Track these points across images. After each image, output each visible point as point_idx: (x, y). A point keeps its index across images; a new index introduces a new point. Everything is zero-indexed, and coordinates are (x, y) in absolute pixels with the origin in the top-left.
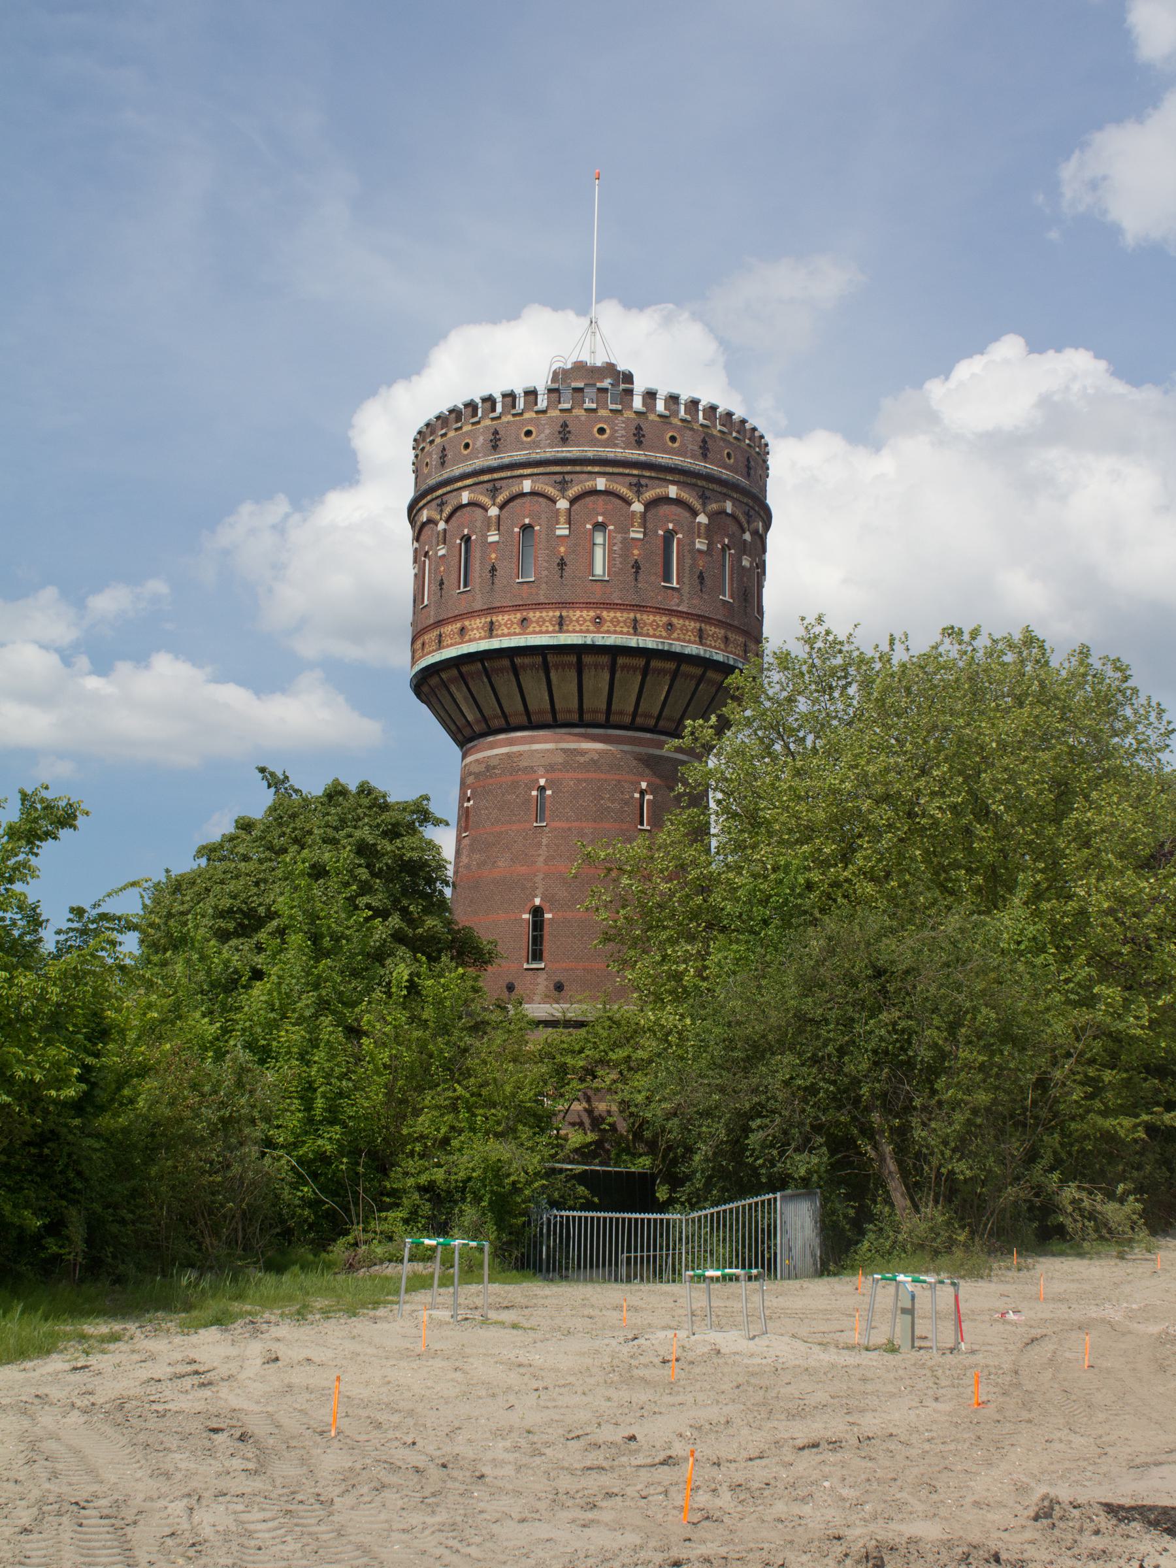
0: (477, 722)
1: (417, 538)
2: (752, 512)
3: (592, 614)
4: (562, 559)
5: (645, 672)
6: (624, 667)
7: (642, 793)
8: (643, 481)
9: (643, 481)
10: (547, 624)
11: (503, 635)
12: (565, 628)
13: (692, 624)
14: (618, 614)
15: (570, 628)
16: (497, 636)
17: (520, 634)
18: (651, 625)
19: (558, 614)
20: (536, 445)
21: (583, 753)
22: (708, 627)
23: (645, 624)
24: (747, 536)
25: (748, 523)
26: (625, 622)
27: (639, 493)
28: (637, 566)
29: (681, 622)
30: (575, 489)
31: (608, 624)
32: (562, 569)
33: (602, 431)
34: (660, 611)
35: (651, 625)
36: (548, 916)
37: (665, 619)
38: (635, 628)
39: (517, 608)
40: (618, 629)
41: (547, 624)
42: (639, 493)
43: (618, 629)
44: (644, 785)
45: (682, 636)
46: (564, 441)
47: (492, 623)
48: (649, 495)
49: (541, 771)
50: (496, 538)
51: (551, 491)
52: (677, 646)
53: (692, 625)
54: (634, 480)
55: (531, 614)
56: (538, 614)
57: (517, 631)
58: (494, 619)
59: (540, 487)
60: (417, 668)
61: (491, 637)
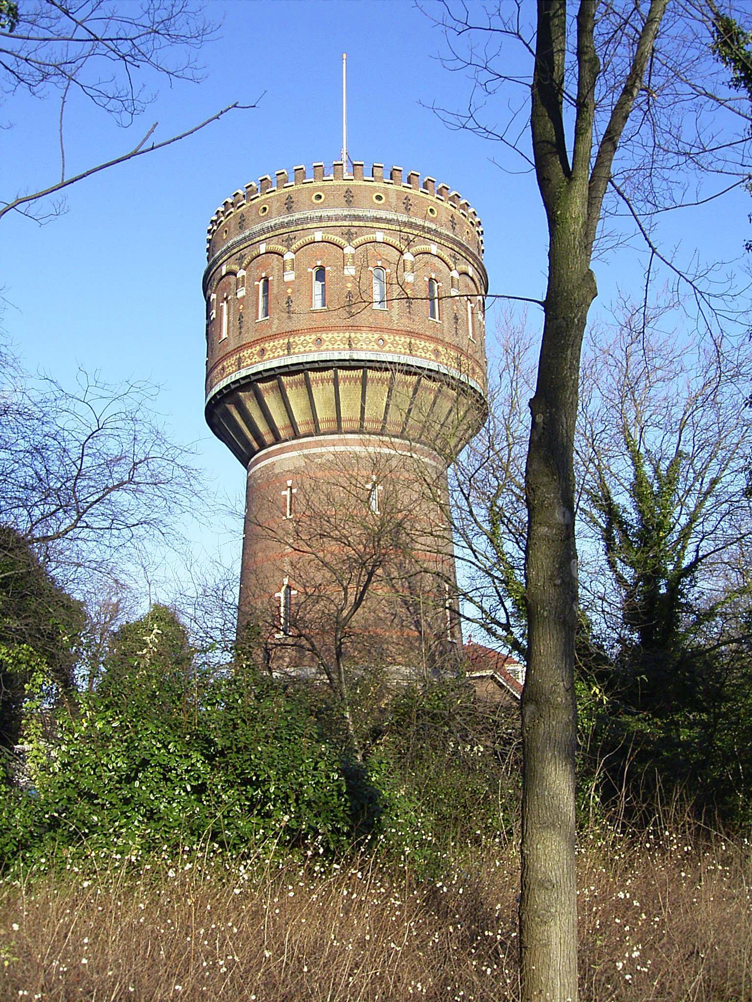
0: (286, 427)
2: (458, 256)
4: (289, 298)
5: (364, 381)
6: (345, 379)
8: (353, 230)
9: (353, 230)
10: (279, 350)
11: (299, 353)
12: (292, 351)
14: (336, 335)
16: (294, 353)
17: (259, 362)
19: (286, 341)
23: (359, 341)
26: (341, 340)
27: (349, 240)
30: (298, 243)
31: (327, 343)
33: (319, 197)
35: (364, 341)
38: (350, 345)
39: (311, 330)
40: (336, 346)
41: (279, 350)
42: (349, 240)
43: (336, 346)
45: (393, 349)
51: (280, 248)
53: (403, 340)
54: (345, 230)
56: (272, 344)
57: (313, 349)
58: (291, 340)
61: (289, 354)
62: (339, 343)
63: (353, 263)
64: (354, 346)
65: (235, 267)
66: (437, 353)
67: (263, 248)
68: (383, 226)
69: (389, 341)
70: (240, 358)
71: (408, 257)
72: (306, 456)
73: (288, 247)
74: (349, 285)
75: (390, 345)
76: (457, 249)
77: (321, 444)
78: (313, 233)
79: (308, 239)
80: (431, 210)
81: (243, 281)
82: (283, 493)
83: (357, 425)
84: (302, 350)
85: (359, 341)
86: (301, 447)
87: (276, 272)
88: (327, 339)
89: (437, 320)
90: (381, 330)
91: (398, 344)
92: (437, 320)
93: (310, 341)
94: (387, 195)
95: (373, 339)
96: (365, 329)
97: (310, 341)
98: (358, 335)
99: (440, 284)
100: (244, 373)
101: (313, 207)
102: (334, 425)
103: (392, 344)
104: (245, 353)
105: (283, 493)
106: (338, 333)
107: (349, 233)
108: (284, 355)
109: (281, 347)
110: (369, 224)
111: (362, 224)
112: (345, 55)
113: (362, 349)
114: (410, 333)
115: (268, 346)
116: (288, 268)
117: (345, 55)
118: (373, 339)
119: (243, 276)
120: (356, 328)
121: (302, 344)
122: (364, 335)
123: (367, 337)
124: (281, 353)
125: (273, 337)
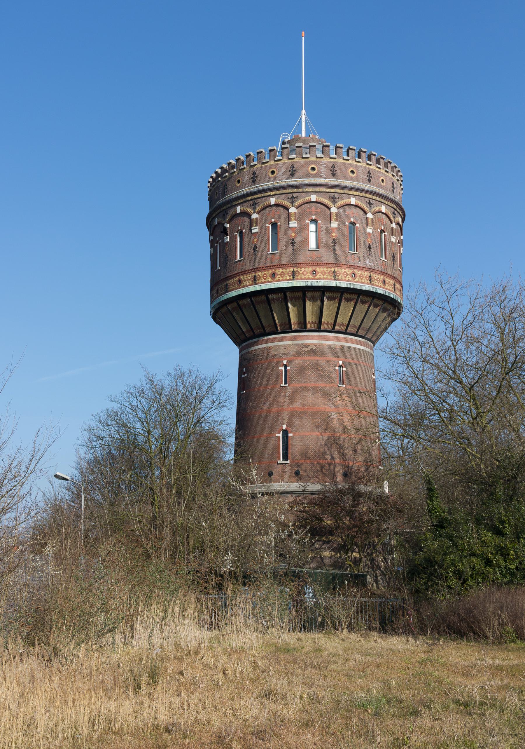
1: (211, 234)
2: (396, 212)
3: (311, 269)
4: (293, 240)
7: (340, 366)
8: (337, 195)
10: (286, 275)
12: (296, 277)
13: (366, 273)
14: (325, 269)
15: (299, 277)
18: (343, 274)
19: (292, 270)
20: (277, 178)
21: (307, 346)
22: (374, 275)
23: (340, 274)
24: (394, 225)
25: (394, 217)
26: (329, 273)
27: (334, 202)
28: (334, 242)
29: (360, 272)
30: (300, 201)
31: (320, 274)
32: (293, 245)
34: (349, 266)
36: (290, 435)
37: (351, 271)
38: (334, 276)
40: (325, 277)
43: (325, 277)
44: (341, 363)
46: (292, 175)
47: (334, 272)
48: (340, 203)
49: (284, 356)
50: (257, 230)
51: (286, 203)
52: (358, 286)
53: (366, 274)
54: (331, 195)
55: (277, 271)
58: (336, 270)
59: (280, 201)
60: (214, 304)
61: (294, 279)
62: (327, 274)
63: (336, 220)
64: (337, 277)
65: (250, 210)
66: (384, 282)
67: (273, 201)
68: (355, 193)
69: (358, 275)
70: (255, 276)
71: (370, 215)
72: (297, 345)
73: (292, 202)
74: (334, 234)
75: (358, 277)
76: (395, 207)
77: (308, 338)
78: (310, 196)
79: (307, 199)
80: (383, 180)
81: (257, 222)
82: (280, 368)
83: (330, 327)
84: (303, 277)
85: (340, 274)
86: (295, 338)
87: (282, 220)
88: (320, 271)
89: (384, 259)
90: (354, 267)
91: (363, 277)
92: (384, 259)
93: (308, 271)
94: (357, 170)
95: (349, 273)
96: (344, 266)
97: (308, 271)
98: (340, 270)
99: (386, 233)
100: (257, 288)
101: (309, 176)
102: (315, 327)
103: (360, 277)
104: (260, 274)
105: (280, 368)
106: (327, 268)
107: (334, 197)
108: (290, 280)
109: (288, 274)
110: (347, 192)
111: (342, 191)
112: (303, 33)
113: (342, 280)
114: (370, 269)
115: (278, 271)
116: (293, 218)
117: (303, 33)
118: (349, 273)
119: (257, 218)
120: (338, 265)
121: (303, 273)
122: (343, 270)
123: (345, 272)
124: (288, 278)
125: (281, 266)
